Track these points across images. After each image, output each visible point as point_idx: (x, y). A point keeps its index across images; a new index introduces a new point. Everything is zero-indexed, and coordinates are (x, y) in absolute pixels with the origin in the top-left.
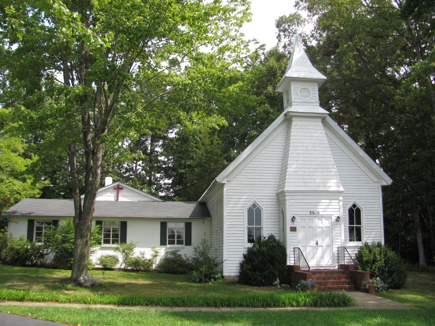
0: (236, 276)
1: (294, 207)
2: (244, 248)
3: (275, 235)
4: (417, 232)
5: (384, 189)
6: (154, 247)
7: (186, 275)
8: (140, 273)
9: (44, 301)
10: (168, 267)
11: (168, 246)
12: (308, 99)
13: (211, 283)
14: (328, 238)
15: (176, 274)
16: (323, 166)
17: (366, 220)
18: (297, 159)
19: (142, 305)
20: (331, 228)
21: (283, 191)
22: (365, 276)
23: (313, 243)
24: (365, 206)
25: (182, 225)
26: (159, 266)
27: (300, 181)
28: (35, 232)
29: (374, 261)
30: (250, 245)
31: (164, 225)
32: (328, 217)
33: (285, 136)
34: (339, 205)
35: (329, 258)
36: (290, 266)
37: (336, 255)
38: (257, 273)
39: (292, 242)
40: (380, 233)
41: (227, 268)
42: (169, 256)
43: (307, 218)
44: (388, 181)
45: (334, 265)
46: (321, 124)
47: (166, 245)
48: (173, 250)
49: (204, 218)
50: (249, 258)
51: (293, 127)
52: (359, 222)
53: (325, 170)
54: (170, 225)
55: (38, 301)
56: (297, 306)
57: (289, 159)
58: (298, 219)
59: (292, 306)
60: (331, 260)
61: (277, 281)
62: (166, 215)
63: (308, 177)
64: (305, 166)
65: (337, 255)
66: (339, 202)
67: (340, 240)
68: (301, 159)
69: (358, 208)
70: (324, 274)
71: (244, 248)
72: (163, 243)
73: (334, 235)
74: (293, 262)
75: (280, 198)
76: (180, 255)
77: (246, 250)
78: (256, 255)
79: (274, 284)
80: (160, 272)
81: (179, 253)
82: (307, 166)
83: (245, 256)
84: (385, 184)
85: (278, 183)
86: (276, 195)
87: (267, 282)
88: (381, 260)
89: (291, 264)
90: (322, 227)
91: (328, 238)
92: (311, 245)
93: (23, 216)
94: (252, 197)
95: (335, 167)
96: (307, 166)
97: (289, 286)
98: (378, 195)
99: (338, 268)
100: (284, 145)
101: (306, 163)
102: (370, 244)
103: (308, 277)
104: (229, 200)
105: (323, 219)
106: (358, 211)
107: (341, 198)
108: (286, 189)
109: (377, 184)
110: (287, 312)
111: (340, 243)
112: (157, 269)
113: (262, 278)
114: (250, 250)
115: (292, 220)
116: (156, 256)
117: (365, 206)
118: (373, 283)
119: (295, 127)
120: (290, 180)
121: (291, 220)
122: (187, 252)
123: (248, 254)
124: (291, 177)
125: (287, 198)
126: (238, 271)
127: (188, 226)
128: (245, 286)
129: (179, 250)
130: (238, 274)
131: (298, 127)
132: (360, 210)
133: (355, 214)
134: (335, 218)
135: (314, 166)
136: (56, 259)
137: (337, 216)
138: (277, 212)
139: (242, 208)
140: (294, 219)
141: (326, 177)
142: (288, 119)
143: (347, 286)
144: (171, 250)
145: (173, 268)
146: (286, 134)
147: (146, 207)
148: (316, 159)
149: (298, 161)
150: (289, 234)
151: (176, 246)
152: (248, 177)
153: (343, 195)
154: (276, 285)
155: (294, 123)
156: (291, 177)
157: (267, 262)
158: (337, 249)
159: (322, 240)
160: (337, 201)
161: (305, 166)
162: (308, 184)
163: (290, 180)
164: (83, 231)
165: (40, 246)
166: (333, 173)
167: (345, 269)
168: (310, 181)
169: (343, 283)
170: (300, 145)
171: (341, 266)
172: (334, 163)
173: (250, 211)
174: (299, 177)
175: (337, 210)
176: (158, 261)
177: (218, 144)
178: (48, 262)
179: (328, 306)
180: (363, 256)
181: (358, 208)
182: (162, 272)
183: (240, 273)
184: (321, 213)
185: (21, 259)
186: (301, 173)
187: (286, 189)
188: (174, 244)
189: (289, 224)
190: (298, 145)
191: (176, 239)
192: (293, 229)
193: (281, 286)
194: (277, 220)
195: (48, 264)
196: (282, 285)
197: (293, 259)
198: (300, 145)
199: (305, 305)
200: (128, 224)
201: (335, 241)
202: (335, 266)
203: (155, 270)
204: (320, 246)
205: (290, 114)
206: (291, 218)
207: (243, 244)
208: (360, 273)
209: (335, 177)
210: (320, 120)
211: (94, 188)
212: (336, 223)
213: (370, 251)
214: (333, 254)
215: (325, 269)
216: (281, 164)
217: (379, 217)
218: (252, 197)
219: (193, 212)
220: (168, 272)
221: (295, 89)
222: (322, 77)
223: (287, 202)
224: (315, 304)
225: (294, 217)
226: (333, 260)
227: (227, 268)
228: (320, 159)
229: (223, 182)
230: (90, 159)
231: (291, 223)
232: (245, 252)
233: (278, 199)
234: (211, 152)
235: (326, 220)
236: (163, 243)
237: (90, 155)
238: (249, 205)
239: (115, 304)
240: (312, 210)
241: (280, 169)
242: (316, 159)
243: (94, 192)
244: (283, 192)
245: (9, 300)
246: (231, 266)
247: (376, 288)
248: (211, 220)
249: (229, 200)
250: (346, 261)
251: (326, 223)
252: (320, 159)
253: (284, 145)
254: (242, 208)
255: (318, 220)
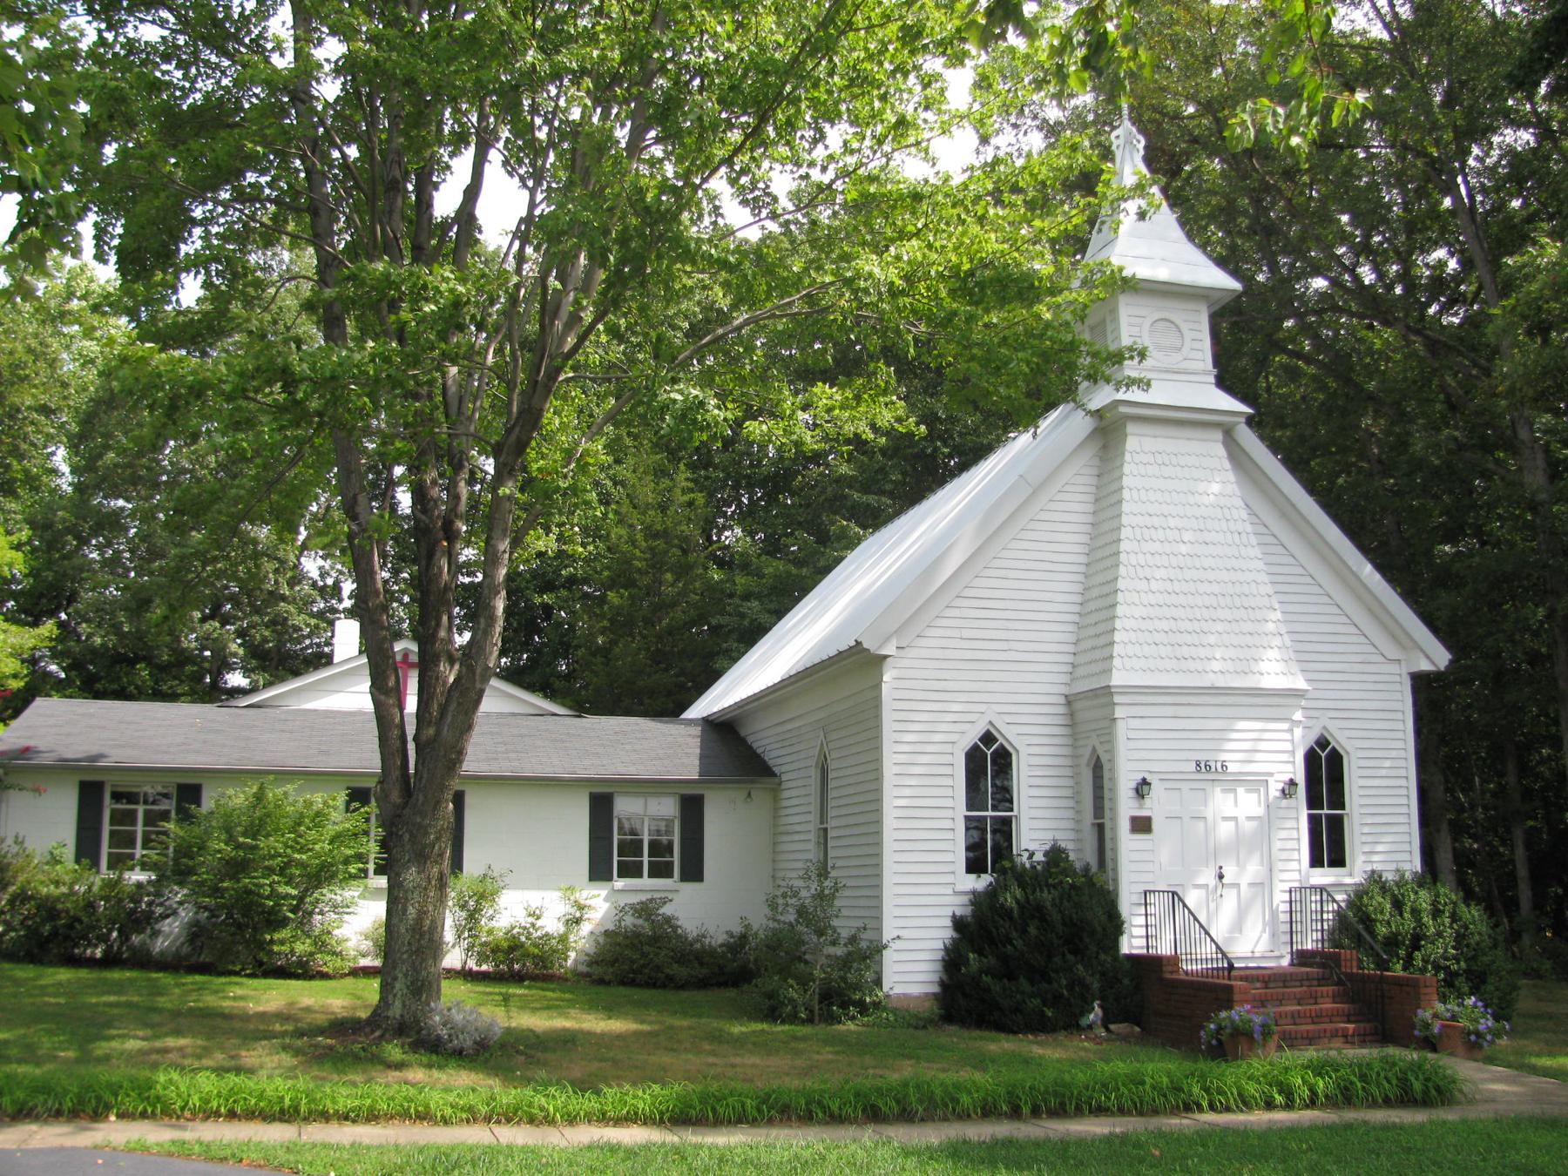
0: (927, 994)
1: (1141, 744)
2: (956, 893)
3: (1070, 846)
4: (1438, 831)
5: (1423, 684)
6: (571, 889)
7: (726, 991)
8: (528, 987)
9: (372, 1117)
10: (633, 962)
11: (619, 883)
12: (1177, 357)
13: (851, 1026)
14: (1256, 858)
15: (664, 986)
16: (1237, 600)
17: (1362, 792)
18: (1148, 572)
19: (755, 1120)
20: (1268, 822)
21: (1109, 687)
22: (1423, 990)
23: (1208, 877)
24: (1359, 744)
25: (668, 808)
26: (595, 961)
27: (1163, 651)
28: (106, 828)
29: (1417, 941)
30: (982, 882)
31: (601, 806)
32: (1256, 783)
33: (1093, 490)
34: (1292, 741)
35: (1260, 927)
36: (1130, 957)
37: (1285, 917)
38: (1024, 984)
39: (1138, 869)
40: (1406, 838)
41: (897, 968)
42: (629, 921)
43: (1185, 786)
44: (1435, 656)
45: (1276, 953)
46: (1221, 451)
47: (610, 879)
48: (644, 897)
49: (752, 782)
50: (976, 932)
51: (1128, 457)
52: (1338, 800)
53: (1242, 613)
54: (625, 807)
55: (346, 1118)
56: (1289, 1106)
57: (1122, 570)
58: (1157, 789)
59: (1270, 1105)
60: (1266, 936)
61: (1095, 1014)
62: (613, 771)
63: (1189, 639)
64: (1173, 599)
65: (1286, 917)
66: (1291, 731)
67: (1294, 865)
68: (1161, 573)
69: (1334, 749)
70: (1258, 985)
71: (956, 893)
72: (599, 871)
73: (1278, 845)
74: (1143, 942)
75: (1087, 714)
76: (668, 920)
77: (965, 899)
78: (1011, 918)
79: (1084, 1022)
80: (601, 982)
81: (667, 910)
82: (1182, 600)
83: (959, 924)
84: (1425, 666)
85: (1070, 659)
86: (1062, 700)
87: (1059, 1018)
88: (1439, 934)
89: (1135, 952)
90: (1235, 819)
91: (1256, 858)
92: (1201, 881)
93: (63, 768)
94: (982, 708)
95: (1277, 606)
96: (1182, 600)
97: (1137, 1029)
98: (1398, 706)
99: (1292, 964)
100: (1090, 519)
101: (1177, 587)
102: (1389, 877)
103: (1236, 997)
104: (902, 716)
105: (1241, 790)
106: (1336, 760)
107: (1298, 715)
108: (1117, 679)
109: (1394, 668)
110: (1243, 1133)
111: (1296, 876)
112: (583, 969)
113: (1044, 1003)
114: (984, 904)
115: (1137, 790)
116: (578, 921)
117: (1359, 744)
118: (1454, 1018)
119: (1137, 458)
120: (1130, 650)
121: (1132, 794)
122: (699, 911)
123: (974, 914)
124: (1133, 636)
125: (1119, 712)
126: (936, 977)
127: (692, 808)
128: (986, 1034)
129: (665, 901)
130: (935, 989)
131: (1145, 458)
132: (1341, 757)
133: (1324, 774)
134: (1281, 786)
135: (1208, 601)
136: (196, 933)
137: (1286, 778)
138: (1067, 762)
139: (948, 748)
140: (1145, 788)
141: (1249, 640)
142: (1108, 432)
143: (1351, 1026)
144: (634, 899)
145: (640, 965)
146: (1094, 481)
147: (521, 736)
148: (1211, 575)
149: (1153, 582)
150: (1128, 845)
151: (646, 882)
152: (966, 634)
153: (1303, 703)
154: (1090, 1027)
155: (1132, 443)
156: (1133, 636)
157: (1044, 943)
158: (1286, 897)
159: (1238, 864)
160: (1285, 726)
161: (1173, 599)
162: (1191, 665)
163: (1130, 650)
164: (427, 834)
165: (139, 885)
166: (1271, 627)
167: (1323, 966)
168: (1193, 651)
169: (1330, 1017)
170: (1156, 521)
171: (1302, 958)
172: (1269, 589)
173: (974, 758)
174: (1159, 637)
175: (1285, 757)
176: (582, 940)
177: (690, 504)
178: (160, 945)
179: (1388, 1103)
180: (1375, 921)
181: (1334, 750)
182: (608, 983)
183: (942, 983)
184: (1232, 768)
185: (52, 935)
186: (1164, 625)
187: (1117, 679)
188: (641, 876)
189: (1126, 807)
190: (1148, 521)
191: (646, 859)
192: (1142, 825)
193: (1108, 1030)
194: (1068, 793)
195: (162, 953)
196: (1112, 1027)
197: (1142, 932)
198: (1156, 521)
199: (1312, 1103)
200: (469, 800)
201: (1280, 865)
202: (1282, 957)
203: (575, 972)
204: (1225, 886)
205: (1123, 409)
206: (1133, 785)
207: (950, 879)
208: (1398, 982)
209: (1277, 641)
210: (1219, 435)
211: (478, 671)
212: (1284, 803)
213: (1398, 905)
214: (1274, 913)
215: (1247, 968)
216: (1079, 588)
217: (1403, 782)
218: (982, 708)
219: (702, 757)
220: (632, 983)
221: (1133, 320)
222: (1225, 281)
223: (1121, 728)
224: (1345, 1097)
225: (1144, 782)
226: (1273, 935)
227: (897, 968)
228: (1225, 576)
229: (884, 652)
230: (438, 554)
231: (1133, 803)
232: (959, 906)
233: (1072, 715)
234: (664, 534)
235: (1249, 791)
236: (599, 871)
237: (438, 542)
238: (972, 736)
239: (647, 1121)
240: (1202, 757)
241: (1077, 609)
242: (1211, 575)
243: (478, 686)
244: (1105, 694)
245: (232, 1115)
246: (910, 965)
247: (1469, 1033)
248: (776, 791)
249: (902, 716)
250: (1310, 942)
251: (1248, 805)
252: (1225, 576)
253: (1090, 519)
254: (948, 748)
255: (1224, 791)
